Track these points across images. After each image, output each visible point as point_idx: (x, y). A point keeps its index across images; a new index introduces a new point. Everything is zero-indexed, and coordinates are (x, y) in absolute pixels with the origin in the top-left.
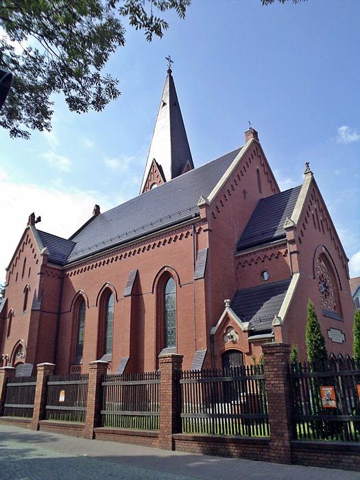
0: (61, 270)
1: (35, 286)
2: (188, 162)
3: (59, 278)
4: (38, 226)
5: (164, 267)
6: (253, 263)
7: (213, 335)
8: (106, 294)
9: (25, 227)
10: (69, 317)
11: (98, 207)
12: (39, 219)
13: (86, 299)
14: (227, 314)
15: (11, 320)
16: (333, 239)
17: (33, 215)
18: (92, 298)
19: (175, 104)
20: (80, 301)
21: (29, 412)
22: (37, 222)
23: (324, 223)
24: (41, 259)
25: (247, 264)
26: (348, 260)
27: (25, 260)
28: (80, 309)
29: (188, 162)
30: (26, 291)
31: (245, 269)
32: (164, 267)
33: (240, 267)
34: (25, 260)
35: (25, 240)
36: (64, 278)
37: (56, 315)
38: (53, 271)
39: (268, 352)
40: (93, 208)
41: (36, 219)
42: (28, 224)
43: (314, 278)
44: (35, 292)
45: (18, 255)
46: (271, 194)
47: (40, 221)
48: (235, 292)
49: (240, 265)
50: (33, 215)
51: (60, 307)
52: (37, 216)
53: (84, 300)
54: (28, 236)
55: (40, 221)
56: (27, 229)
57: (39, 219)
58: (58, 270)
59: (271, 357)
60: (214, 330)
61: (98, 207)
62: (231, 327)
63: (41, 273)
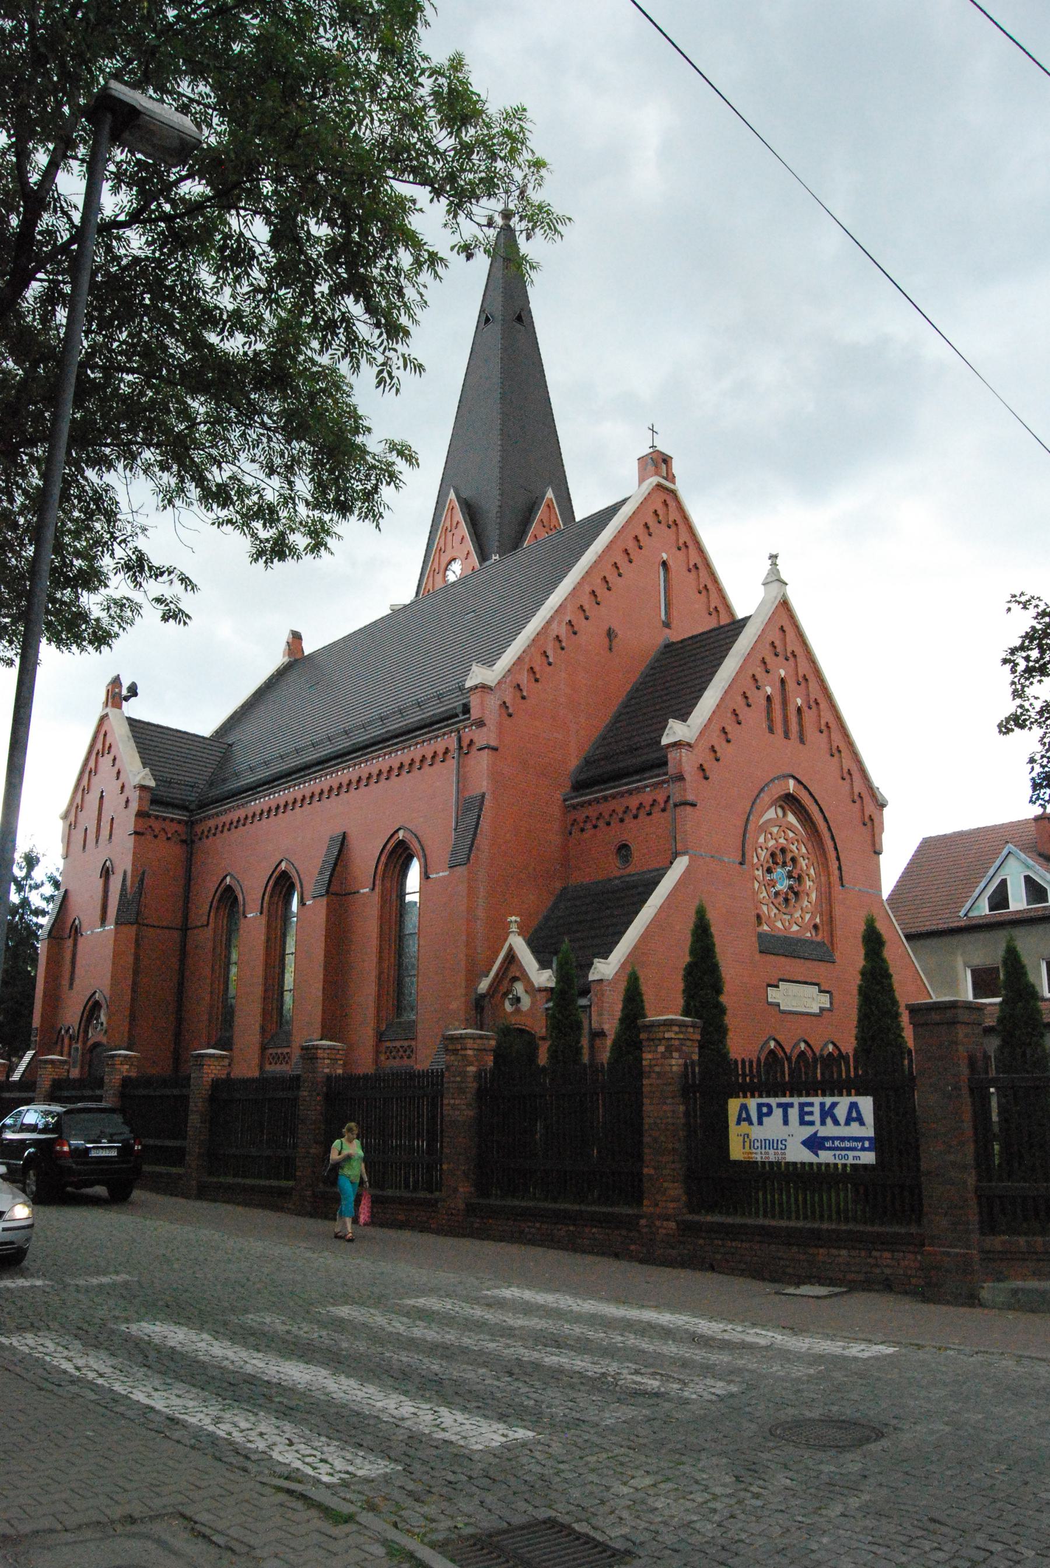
0: (186, 823)
1: (124, 863)
2: (550, 494)
3: (183, 841)
4: (133, 709)
5: (397, 831)
6: (601, 824)
7: (483, 996)
8: (283, 884)
9: (98, 711)
10: (204, 938)
11: (296, 636)
12: (133, 691)
13: (240, 898)
14: (511, 948)
15: (75, 945)
16: (835, 752)
17: (116, 681)
18: (253, 888)
19: (519, 319)
20: (228, 899)
21: (178, 1156)
22: (126, 699)
23: (809, 716)
24: (134, 796)
25: (588, 826)
26: (883, 806)
27: (102, 797)
28: (641, 748)
29: (550, 494)
30: (106, 873)
31: (586, 835)
32: (397, 831)
33: (575, 830)
34: (102, 797)
35: (99, 746)
36: (193, 842)
37: (180, 932)
38: (166, 825)
39: (450, 1047)
40: (285, 637)
41: (124, 692)
42: (106, 704)
43: (741, 864)
44: (124, 880)
45: (85, 782)
46: (708, 624)
47: (135, 694)
48: (558, 892)
49: (574, 824)
50: (116, 681)
51: (186, 917)
52: (126, 684)
53: (236, 898)
54: (105, 735)
55: (135, 694)
56: (103, 719)
57: (133, 691)
58: (180, 822)
59: (452, 1058)
60: (484, 985)
61: (296, 636)
62: (515, 979)
63: (136, 833)
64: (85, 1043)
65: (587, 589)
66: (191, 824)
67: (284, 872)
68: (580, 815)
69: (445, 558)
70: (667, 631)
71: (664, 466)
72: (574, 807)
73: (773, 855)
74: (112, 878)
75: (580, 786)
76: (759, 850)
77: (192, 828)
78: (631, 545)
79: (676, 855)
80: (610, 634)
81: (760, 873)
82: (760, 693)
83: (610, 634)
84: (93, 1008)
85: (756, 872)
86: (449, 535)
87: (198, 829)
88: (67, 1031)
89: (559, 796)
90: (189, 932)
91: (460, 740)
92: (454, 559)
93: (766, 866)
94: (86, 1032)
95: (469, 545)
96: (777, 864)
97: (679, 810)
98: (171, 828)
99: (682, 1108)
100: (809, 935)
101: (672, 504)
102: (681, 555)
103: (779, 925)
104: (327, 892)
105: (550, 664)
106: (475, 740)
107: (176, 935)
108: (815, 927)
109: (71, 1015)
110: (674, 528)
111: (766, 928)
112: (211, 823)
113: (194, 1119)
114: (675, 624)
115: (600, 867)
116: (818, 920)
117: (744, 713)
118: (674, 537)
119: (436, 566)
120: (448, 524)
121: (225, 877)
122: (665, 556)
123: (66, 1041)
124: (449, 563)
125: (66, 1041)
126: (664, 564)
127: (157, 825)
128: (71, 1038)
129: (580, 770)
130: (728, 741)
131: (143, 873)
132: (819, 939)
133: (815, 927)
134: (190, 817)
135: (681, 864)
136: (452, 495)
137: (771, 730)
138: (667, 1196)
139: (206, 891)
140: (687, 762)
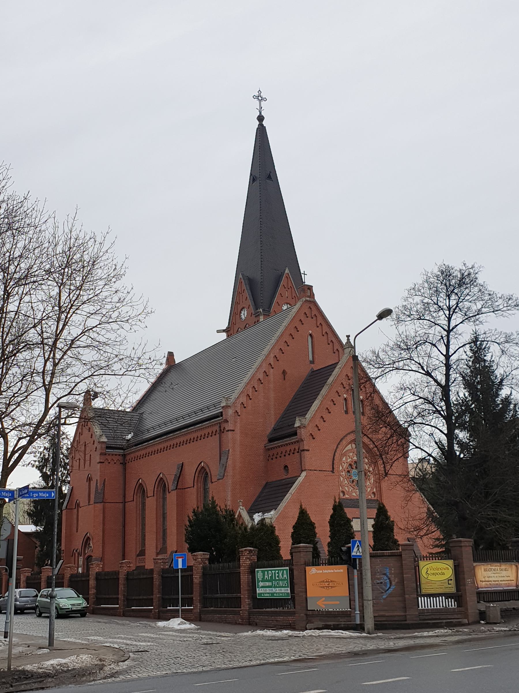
1: (97, 477)
11: (171, 355)
20: (141, 489)
30: (89, 479)
36: (126, 463)
44: (97, 483)
64: (84, 556)
65: (272, 355)
66: (124, 456)
67: (162, 478)
68: (271, 453)
69: (240, 308)
70: (312, 365)
71: (309, 291)
72: (269, 449)
73: (350, 465)
74: (92, 482)
75: (271, 440)
76: (343, 464)
77: (125, 457)
78: (293, 332)
79: (302, 471)
80: (284, 372)
81: (344, 473)
82: (341, 398)
83: (284, 372)
84: (87, 541)
85: (342, 473)
86: (241, 295)
87: (128, 457)
88: (76, 551)
89: (262, 446)
90: (126, 504)
91: (220, 427)
92: (244, 308)
93: (346, 470)
94: (85, 551)
95: (250, 302)
96: (352, 468)
97: (302, 453)
98: (115, 458)
99: (250, 576)
100: (370, 497)
101: (313, 308)
102: (319, 329)
103: (354, 494)
104: (176, 489)
105: (256, 391)
106: (226, 427)
107: (121, 505)
108: (374, 493)
109: (78, 544)
110: (315, 318)
111: (347, 496)
112: (132, 455)
113: (121, 587)
114: (316, 361)
115: (280, 475)
116: (375, 490)
117: (332, 408)
118: (315, 322)
119: (236, 311)
120: (240, 290)
121: (139, 480)
122: (310, 332)
123: (76, 555)
124: (242, 310)
125: (76, 555)
126: (310, 335)
127: (109, 458)
128: (78, 554)
129: (271, 434)
130: (324, 421)
131: (105, 480)
132: (376, 498)
133: (374, 493)
134: (123, 452)
135: (304, 474)
136: (241, 276)
137: (346, 412)
138: (246, 603)
139: (132, 485)
140: (303, 433)
